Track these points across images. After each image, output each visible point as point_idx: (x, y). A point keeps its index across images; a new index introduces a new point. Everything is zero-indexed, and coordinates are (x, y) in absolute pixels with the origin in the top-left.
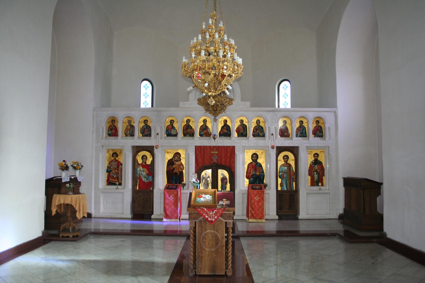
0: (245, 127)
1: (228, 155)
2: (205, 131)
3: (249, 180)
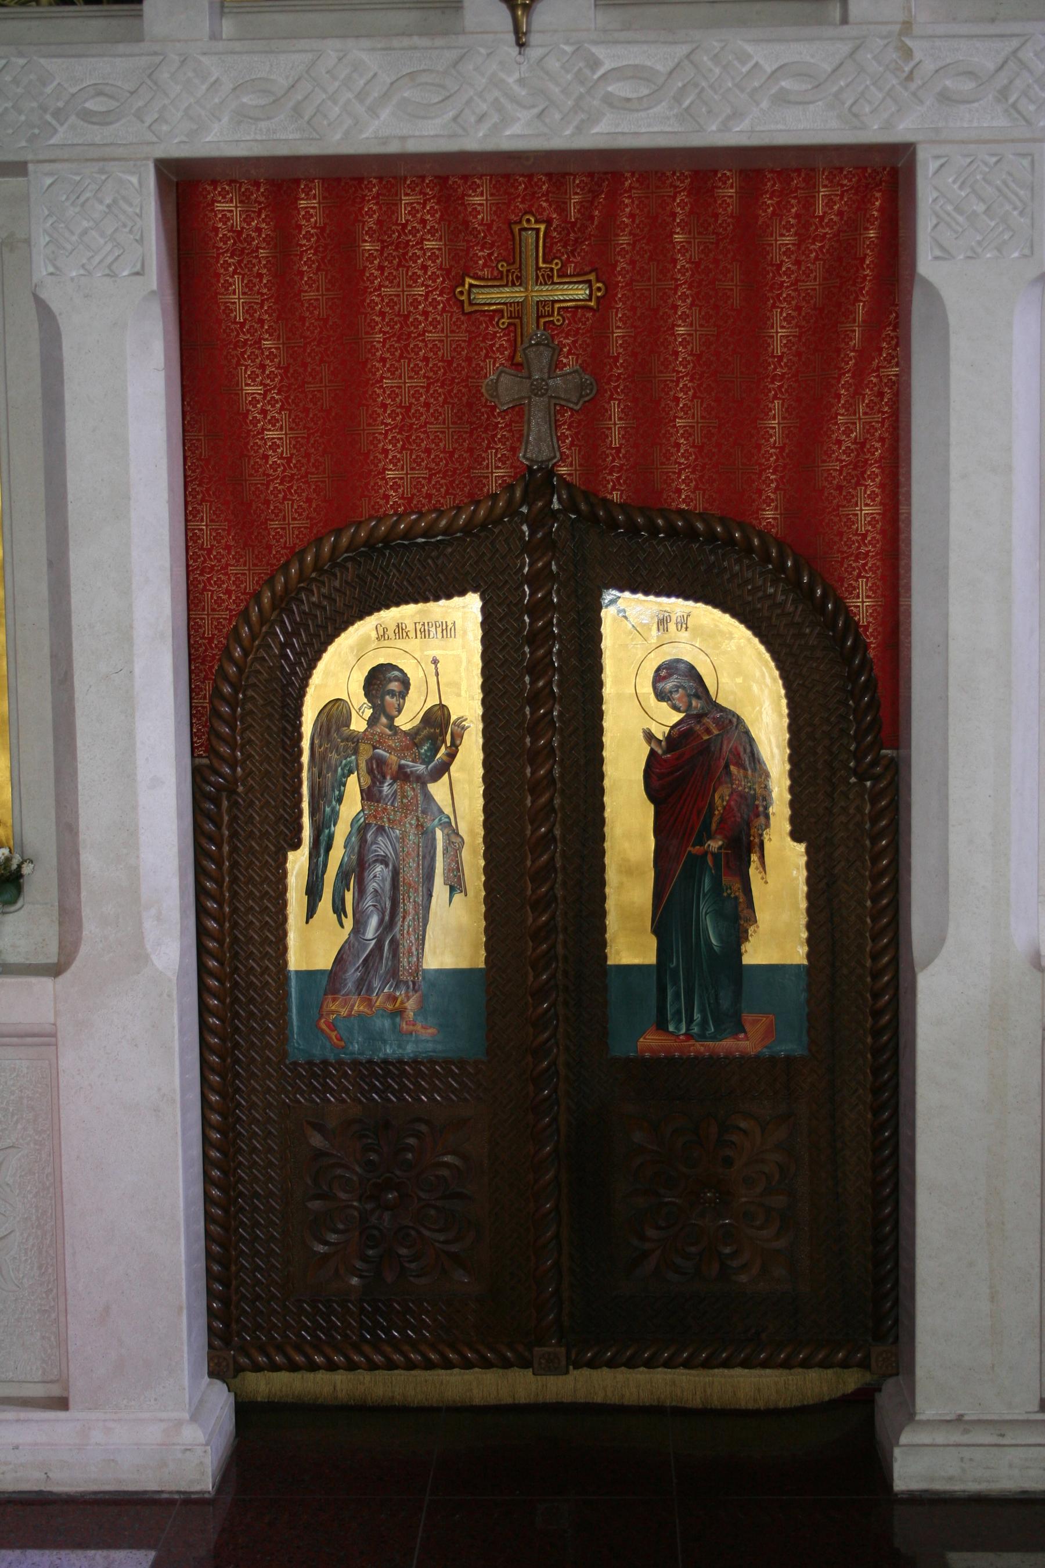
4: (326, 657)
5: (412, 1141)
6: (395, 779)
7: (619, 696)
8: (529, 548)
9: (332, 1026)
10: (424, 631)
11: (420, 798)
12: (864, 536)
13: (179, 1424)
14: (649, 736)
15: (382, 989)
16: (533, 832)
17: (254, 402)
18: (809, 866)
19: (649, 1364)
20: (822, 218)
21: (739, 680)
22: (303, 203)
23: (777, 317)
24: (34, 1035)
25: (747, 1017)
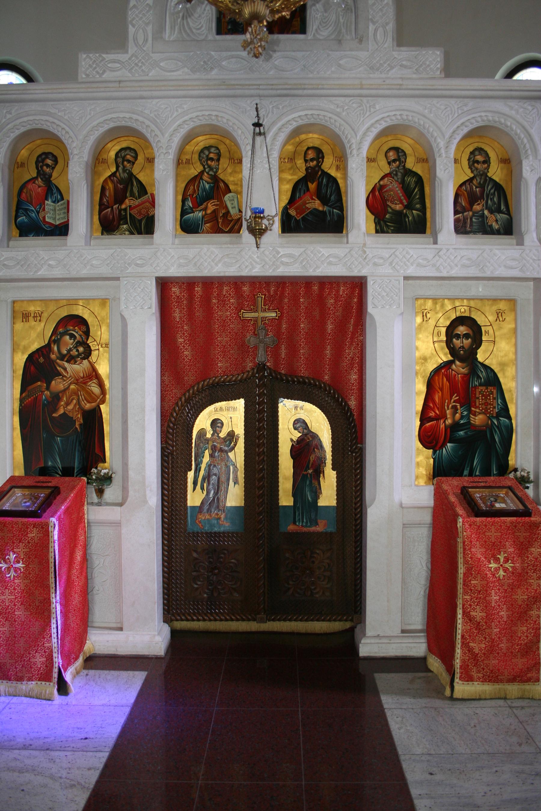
0: (412, 185)
1: (330, 327)
2: (211, 207)
3: (434, 453)
4: (200, 416)
5: (222, 555)
6: (219, 452)
7: (283, 428)
8: (258, 386)
9: (200, 522)
10: (228, 409)
11: (226, 457)
12: (353, 384)
13: (154, 636)
14: (292, 440)
15: (214, 512)
16: (259, 467)
17: (181, 344)
18: (337, 477)
19: (290, 620)
20: (341, 295)
21: (318, 424)
22: (196, 289)
23: (329, 322)
24: (114, 523)
25: (319, 521)
